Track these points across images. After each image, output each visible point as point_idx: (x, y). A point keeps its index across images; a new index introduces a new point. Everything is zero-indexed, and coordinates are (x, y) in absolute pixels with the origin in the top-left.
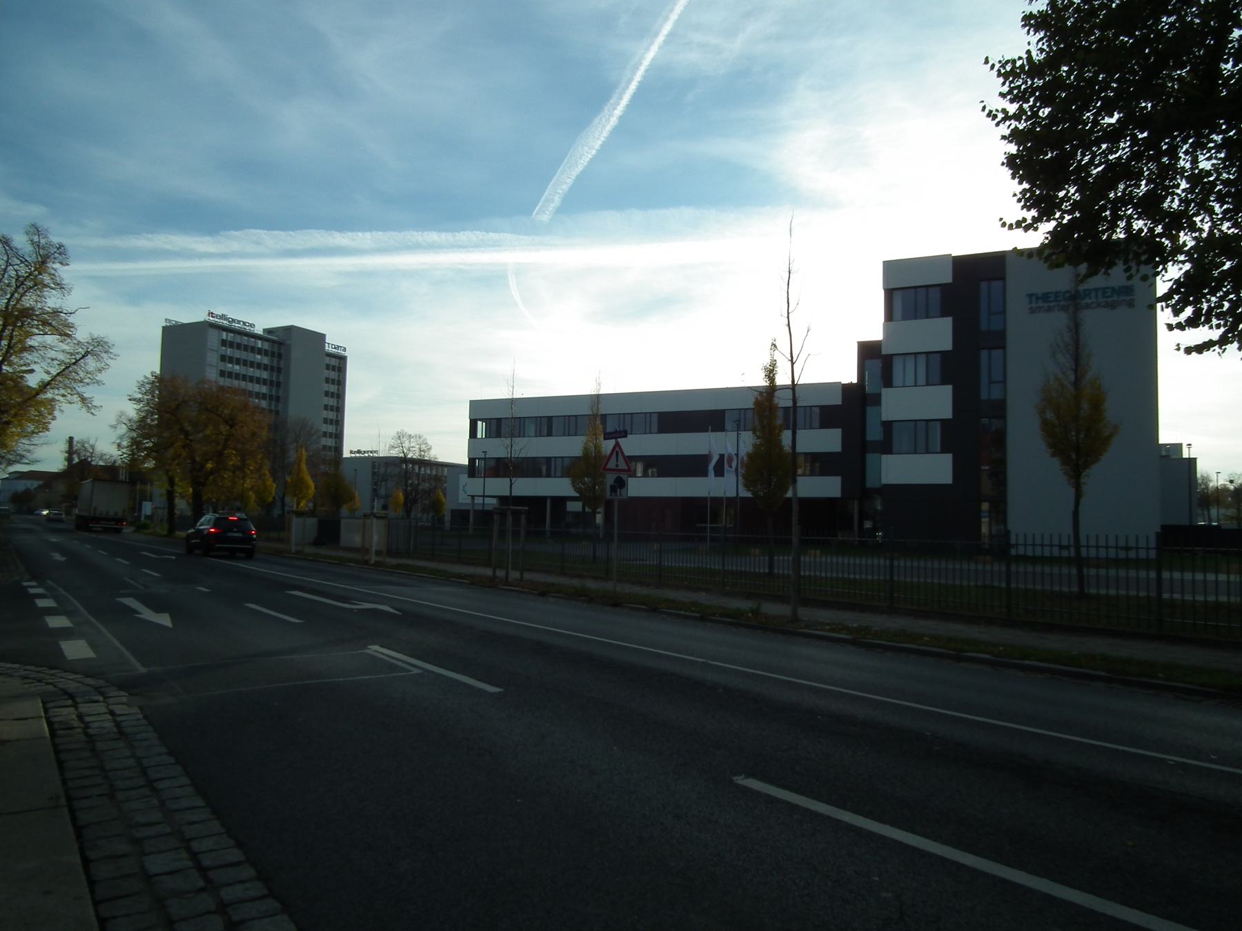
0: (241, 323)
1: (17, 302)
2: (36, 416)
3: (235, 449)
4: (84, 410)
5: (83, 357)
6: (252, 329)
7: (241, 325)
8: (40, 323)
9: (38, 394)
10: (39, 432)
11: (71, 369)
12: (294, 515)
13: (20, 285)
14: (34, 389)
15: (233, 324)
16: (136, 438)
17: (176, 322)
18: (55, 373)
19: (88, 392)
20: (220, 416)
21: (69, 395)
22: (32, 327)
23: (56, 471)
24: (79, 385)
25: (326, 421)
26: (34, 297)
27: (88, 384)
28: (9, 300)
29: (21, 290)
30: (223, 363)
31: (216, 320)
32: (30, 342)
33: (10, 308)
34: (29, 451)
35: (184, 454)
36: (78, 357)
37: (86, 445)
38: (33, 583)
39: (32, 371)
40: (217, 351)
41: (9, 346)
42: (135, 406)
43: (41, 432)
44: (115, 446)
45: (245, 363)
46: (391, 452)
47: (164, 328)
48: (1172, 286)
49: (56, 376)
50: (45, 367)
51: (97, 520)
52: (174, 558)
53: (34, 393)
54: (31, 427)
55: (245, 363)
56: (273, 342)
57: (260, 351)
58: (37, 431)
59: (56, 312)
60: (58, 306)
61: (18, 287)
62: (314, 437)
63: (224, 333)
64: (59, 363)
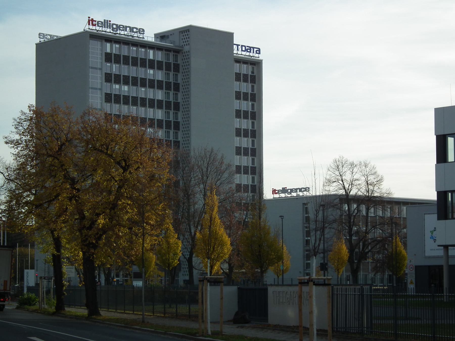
0: (128, 29)
3: (130, 198)
6: (141, 36)
12: (209, 284)
15: (118, 32)
17: (50, 36)
20: (111, 156)
25: (238, 151)
30: (109, 84)
31: (98, 28)
35: (70, 208)
40: (101, 69)
45: (135, 82)
55: (135, 82)
56: (168, 50)
57: (152, 64)
62: (226, 175)
63: (108, 45)
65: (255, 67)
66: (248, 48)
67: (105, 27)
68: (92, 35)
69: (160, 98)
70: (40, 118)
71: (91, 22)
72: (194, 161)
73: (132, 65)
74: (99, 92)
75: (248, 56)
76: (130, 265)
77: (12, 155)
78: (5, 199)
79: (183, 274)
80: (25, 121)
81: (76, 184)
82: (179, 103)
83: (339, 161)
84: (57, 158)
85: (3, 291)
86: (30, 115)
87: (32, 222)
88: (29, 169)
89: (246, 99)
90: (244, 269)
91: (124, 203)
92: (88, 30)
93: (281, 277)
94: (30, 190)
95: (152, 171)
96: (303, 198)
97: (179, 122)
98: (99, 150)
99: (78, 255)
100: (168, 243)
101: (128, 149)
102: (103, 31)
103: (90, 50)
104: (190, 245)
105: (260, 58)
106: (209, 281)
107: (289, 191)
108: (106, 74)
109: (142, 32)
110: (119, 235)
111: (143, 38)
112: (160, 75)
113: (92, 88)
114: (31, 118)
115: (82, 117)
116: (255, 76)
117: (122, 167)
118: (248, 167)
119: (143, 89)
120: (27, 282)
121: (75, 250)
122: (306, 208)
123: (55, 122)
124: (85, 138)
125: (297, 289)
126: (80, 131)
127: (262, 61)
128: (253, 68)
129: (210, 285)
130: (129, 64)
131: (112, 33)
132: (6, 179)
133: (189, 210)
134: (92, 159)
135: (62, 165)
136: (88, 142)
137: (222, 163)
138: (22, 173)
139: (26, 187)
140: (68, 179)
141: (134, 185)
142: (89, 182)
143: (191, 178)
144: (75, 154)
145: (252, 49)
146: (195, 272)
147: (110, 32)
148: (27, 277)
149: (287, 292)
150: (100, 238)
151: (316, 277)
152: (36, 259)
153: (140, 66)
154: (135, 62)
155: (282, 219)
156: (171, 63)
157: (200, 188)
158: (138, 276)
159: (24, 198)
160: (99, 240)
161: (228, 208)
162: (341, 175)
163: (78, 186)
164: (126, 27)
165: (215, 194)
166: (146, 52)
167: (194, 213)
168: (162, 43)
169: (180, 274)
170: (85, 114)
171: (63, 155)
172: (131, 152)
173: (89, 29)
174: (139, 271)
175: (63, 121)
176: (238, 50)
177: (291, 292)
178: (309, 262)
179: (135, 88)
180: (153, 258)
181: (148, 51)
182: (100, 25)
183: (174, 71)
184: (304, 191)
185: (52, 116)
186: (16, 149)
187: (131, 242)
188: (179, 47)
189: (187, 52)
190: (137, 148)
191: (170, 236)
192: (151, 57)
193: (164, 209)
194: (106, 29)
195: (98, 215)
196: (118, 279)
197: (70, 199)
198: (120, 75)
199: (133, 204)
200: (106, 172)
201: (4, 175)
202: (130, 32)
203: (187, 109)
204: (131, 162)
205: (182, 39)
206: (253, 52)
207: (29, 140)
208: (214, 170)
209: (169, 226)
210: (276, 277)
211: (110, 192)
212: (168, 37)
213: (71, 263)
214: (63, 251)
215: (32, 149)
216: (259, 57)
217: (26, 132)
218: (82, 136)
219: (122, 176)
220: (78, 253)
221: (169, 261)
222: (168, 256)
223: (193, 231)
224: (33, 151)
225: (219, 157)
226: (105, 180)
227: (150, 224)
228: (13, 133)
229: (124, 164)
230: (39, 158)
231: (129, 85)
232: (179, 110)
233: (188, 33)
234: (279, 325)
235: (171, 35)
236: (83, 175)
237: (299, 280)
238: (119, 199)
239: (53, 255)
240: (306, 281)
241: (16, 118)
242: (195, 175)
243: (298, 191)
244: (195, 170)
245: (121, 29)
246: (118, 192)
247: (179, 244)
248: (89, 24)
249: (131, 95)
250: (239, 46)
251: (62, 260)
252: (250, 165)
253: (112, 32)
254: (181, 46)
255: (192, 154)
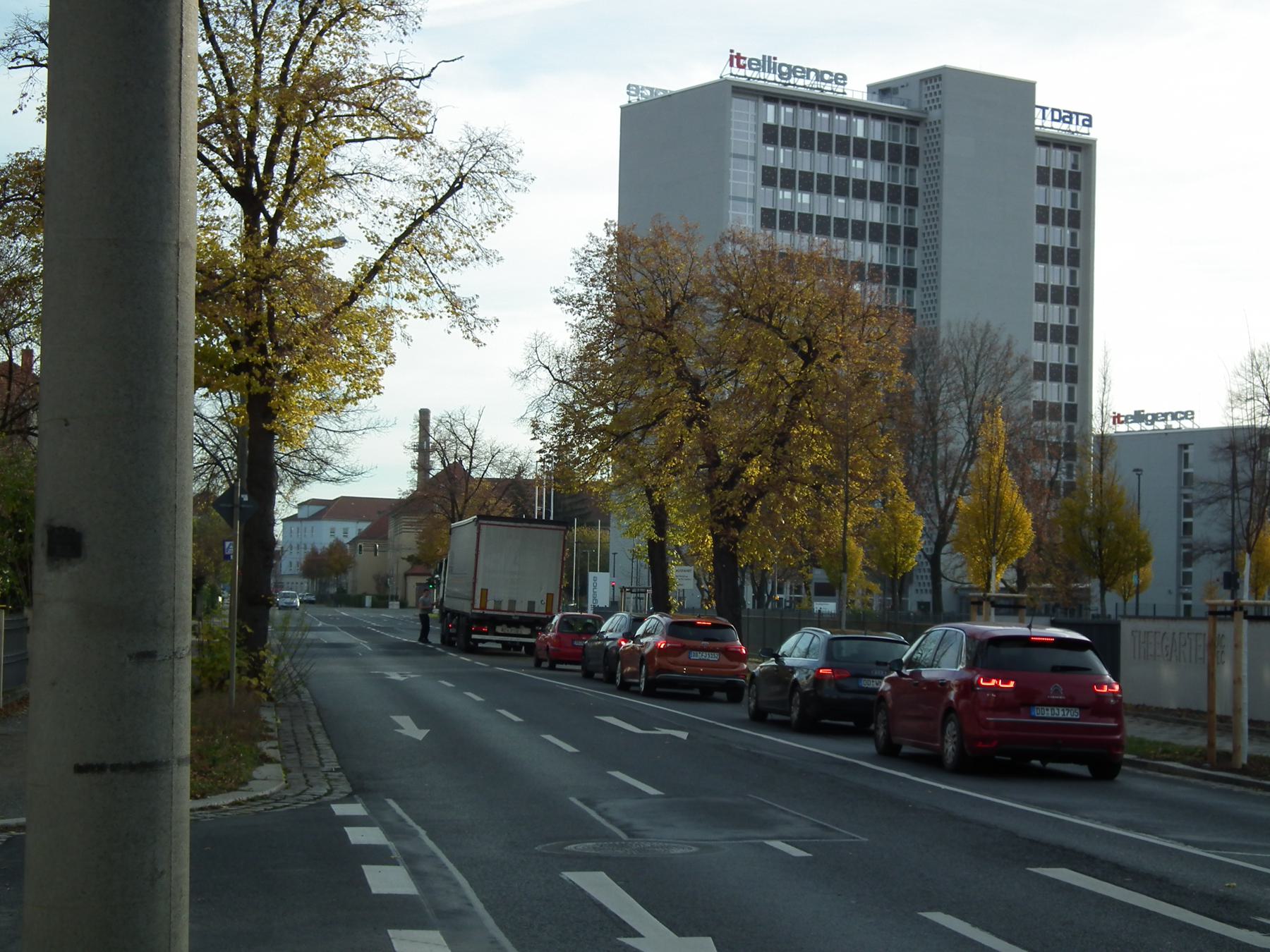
0: (812, 74)
1: (305, 62)
2: (350, 355)
3: (817, 421)
4: (458, 332)
5: (452, 190)
6: (840, 89)
7: (811, 81)
8: (355, 110)
9: (354, 297)
10: (359, 396)
11: (424, 224)
12: (993, 610)
13: (311, 17)
14: (345, 284)
15: (792, 81)
16: (572, 405)
17: (651, 89)
18: (390, 241)
19: (463, 281)
20: (778, 330)
21: (422, 295)
22: (337, 123)
23: (397, 497)
24: (445, 265)
25: (1040, 332)
26: (340, 45)
27: (465, 262)
28: (288, 59)
29: (311, 31)
30: (770, 190)
31: (749, 73)
32: (336, 164)
33: (289, 78)
34: (337, 448)
35: (689, 444)
36: (441, 191)
37: (460, 430)
38: (356, 809)
39: (339, 242)
40: (754, 158)
41: (291, 178)
42: (571, 318)
43: (364, 397)
44: (527, 428)
45: (824, 185)
46: (1237, 413)
47: (624, 109)
48: (1132, 422)
49: (392, 248)
50: (369, 226)
51: (490, 622)
52: (683, 735)
53: (346, 295)
54: (340, 386)
55: (824, 185)
56: (895, 118)
57: (861, 148)
58: (354, 395)
59: (390, 78)
60: (392, 62)
61: (305, 23)
62: (1016, 381)
63: (771, 108)
64: (398, 211)
65: (1080, 155)
66: (1066, 114)
67: (764, 71)
68: (737, 88)
69: (877, 219)
70: (630, 249)
71: (735, 60)
72: (947, 352)
73: (819, 150)
74: (748, 206)
75: (1065, 131)
76: (809, 567)
77: (569, 327)
78: (553, 422)
79: (917, 590)
80: (597, 256)
81: (703, 391)
82: (916, 230)
83: (1260, 355)
84: (662, 334)
85: (545, 616)
86: (608, 244)
87: (608, 471)
88: (603, 358)
89: (1058, 221)
90: (1051, 582)
91: (803, 433)
92: (729, 76)
93: (1132, 601)
94: (602, 404)
95: (866, 365)
96: (1181, 433)
97: (916, 270)
98: (752, 318)
99: (704, 541)
100: (894, 519)
101: (816, 317)
102: (759, 79)
103: (733, 120)
104: (937, 528)
105: (1091, 136)
106: (993, 604)
107: (1150, 418)
108: (764, 168)
109: (842, 82)
110: (792, 501)
111: (844, 93)
112: (877, 172)
113: (735, 198)
114: (611, 249)
115: (718, 247)
116: (1079, 175)
117: (802, 355)
118: (1060, 366)
119: (841, 201)
120: (595, 598)
121: (697, 530)
122: (1186, 456)
123: (661, 258)
124: (724, 291)
125: (1203, 627)
126: (714, 276)
127: (1094, 141)
128: (1076, 157)
129: (996, 614)
130: (812, 148)
131: (779, 83)
132: (555, 380)
133: (935, 453)
134: (738, 336)
135: (674, 351)
136: (729, 301)
137: (1008, 355)
138: (587, 365)
139: (598, 397)
140: (687, 379)
141: (828, 393)
142: (730, 385)
143: (942, 386)
144: (702, 327)
145: (1074, 116)
146: (946, 585)
147: (775, 82)
148: (595, 587)
149: (1164, 634)
150: (750, 508)
151: (1252, 601)
152: (611, 552)
153: (837, 153)
154: (825, 142)
155: (1139, 475)
156: (901, 146)
157: (959, 408)
158: (825, 591)
159: (593, 419)
160: (749, 512)
161: (1020, 450)
162: (1264, 386)
163: (706, 396)
164: (809, 70)
165: (1001, 417)
166: (849, 123)
167: (946, 461)
168: (883, 104)
169: (911, 590)
170: (724, 239)
171: (675, 328)
172: (822, 322)
173: (731, 74)
174: (827, 582)
175: (677, 256)
176: (1044, 118)
177: (1174, 634)
178: (1189, 570)
179: (824, 197)
180: (857, 552)
181: (854, 120)
182: (754, 67)
183: (907, 163)
184: (1182, 418)
185: (655, 245)
186: (577, 315)
187: (815, 515)
188: (918, 112)
189: (935, 122)
190: (836, 315)
191: (899, 507)
192: (860, 134)
193: (888, 449)
194: (767, 74)
195: (748, 457)
196: (782, 596)
197: (689, 423)
198: (794, 172)
199: (825, 434)
200: (769, 364)
201: (550, 372)
202: (817, 80)
203: (933, 243)
204: (821, 344)
205: (926, 95)
206: (1077, 124)
207: (605, 297)
208: (990, 370)
209: (898, 484)
210: (1121, 601)
211: (774, 409)
212: (896, 91)
213: (686, 560)
214: (671, 535)
215: (611, 314)
216: (1088, 134)
217: (599, 278)
218: (718, 287)
219: (800, 374)
220: (704, 539)
221: (896, 559)
222: (893, 549)
223: (942, 498)
224: (611, 319)
225: (1003, 341)
226: (763, 383)
227: (859, 479)
228: (571, 281)
229: (805, 348)
230: (625, 333)
231: (812, 191)
232: (915, 245)
233: (938, 82)
234: (1144, 705)
235: (903, 86)
236: (717, 373)
237: (1210, 605)
238: (794, 424)
239: (651, 542)
240: (1229, 609)
241: (579, 248)
242: (950, 380)
243: (1169, 417)
244: (950, 369)
245: (798, 74)
246: (792, 408)
247: (919, 523)
248: (731, 65)
249: (816, 213)
250: (1046, 111)
251: (669, 552)
252: (1065, 362)
253: (778, 80)
254: (923, 109)
255: (943, 335)
